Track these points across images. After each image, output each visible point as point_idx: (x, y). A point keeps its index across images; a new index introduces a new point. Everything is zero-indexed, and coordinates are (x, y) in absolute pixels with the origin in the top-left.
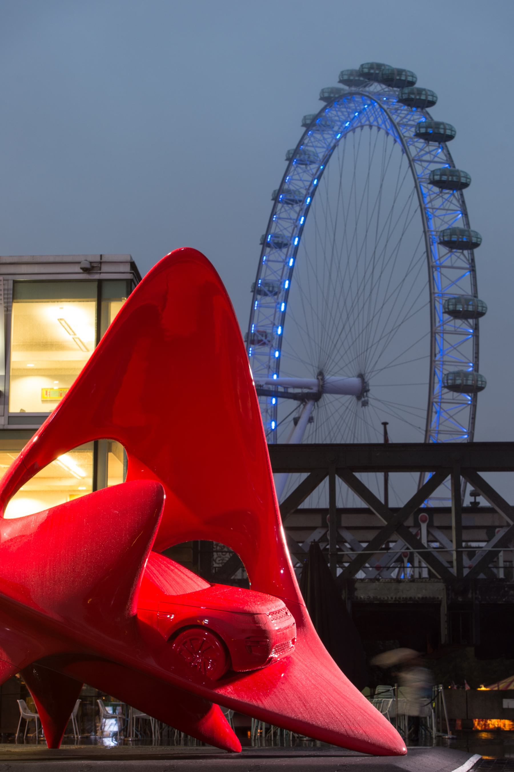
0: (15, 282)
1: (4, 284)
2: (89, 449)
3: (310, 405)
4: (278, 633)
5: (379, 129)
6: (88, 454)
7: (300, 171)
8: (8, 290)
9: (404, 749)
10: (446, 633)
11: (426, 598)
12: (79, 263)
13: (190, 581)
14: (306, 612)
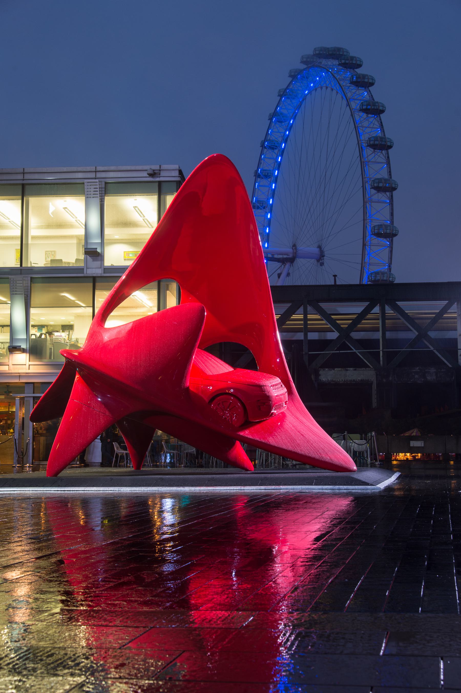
0: (106, 183)
1: (99, 185)
2: (155, 289)
3: (288, 265)
4: (277, 398)
5: (332, 90)
6: (154, 291)
7: (277, 126)
8: (102, 188)
9: (355, 468)
10: (376, 401)
11: (363, 380)
12: (146, 170)
13: (221, 366)
14: (293, 386)
